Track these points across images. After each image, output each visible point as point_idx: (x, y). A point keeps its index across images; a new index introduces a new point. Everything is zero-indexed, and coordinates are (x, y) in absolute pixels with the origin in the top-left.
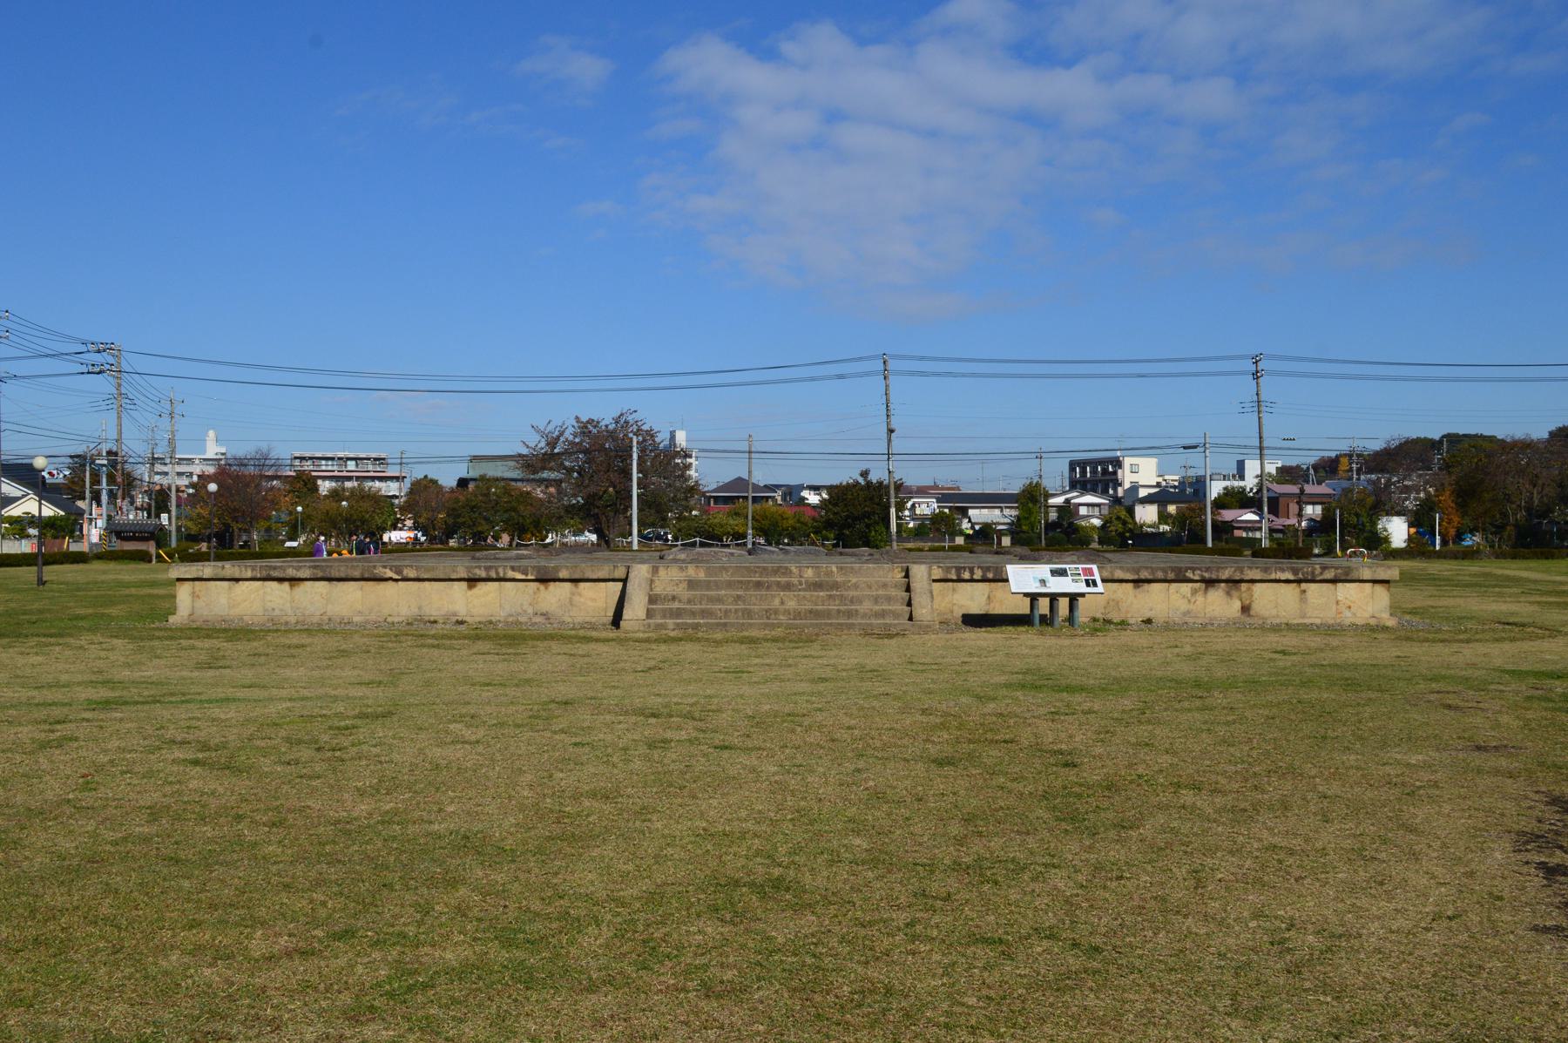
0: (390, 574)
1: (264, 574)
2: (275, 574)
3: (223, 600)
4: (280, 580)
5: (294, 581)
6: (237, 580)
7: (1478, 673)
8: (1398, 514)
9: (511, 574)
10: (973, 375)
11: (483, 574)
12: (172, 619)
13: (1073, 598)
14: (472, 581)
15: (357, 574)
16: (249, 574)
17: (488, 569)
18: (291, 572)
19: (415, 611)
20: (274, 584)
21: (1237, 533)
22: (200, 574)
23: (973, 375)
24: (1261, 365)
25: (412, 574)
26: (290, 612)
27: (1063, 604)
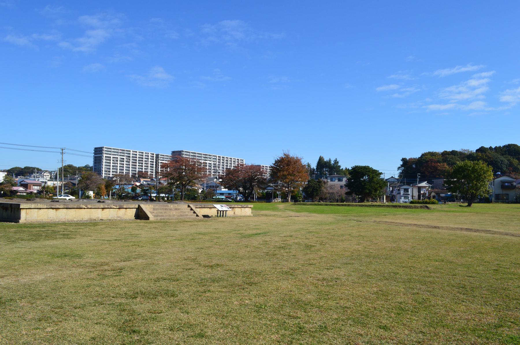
0: (84, 207)
1: (50, 207)
2: (53, 207)
3: (36, 215)
4: (53, 209)
5: (57, 209)
6: (40, 209)
7: (400, 213)
8: (92, 190)
9: (113, 207)
10: (19, 149)
11: (107, 207)
12: (20, 221)
13: (226, 211)
14: (103, 209)
15: (76, 207)
16: (45, 207)
17: (108, 205)
18: (58, 206)
19: (89, 217)
20: (51, 210)
21: (19, 194)
22: (30, 207)
23: (19, 149)
24: (64, 151)
25: (90, 207)
26: (55, 218)
27: (225, 212)
